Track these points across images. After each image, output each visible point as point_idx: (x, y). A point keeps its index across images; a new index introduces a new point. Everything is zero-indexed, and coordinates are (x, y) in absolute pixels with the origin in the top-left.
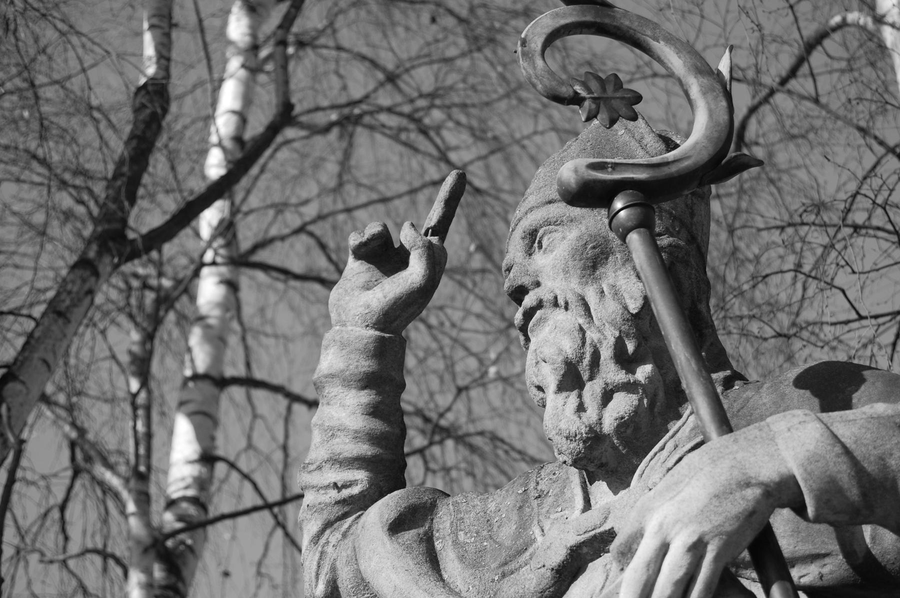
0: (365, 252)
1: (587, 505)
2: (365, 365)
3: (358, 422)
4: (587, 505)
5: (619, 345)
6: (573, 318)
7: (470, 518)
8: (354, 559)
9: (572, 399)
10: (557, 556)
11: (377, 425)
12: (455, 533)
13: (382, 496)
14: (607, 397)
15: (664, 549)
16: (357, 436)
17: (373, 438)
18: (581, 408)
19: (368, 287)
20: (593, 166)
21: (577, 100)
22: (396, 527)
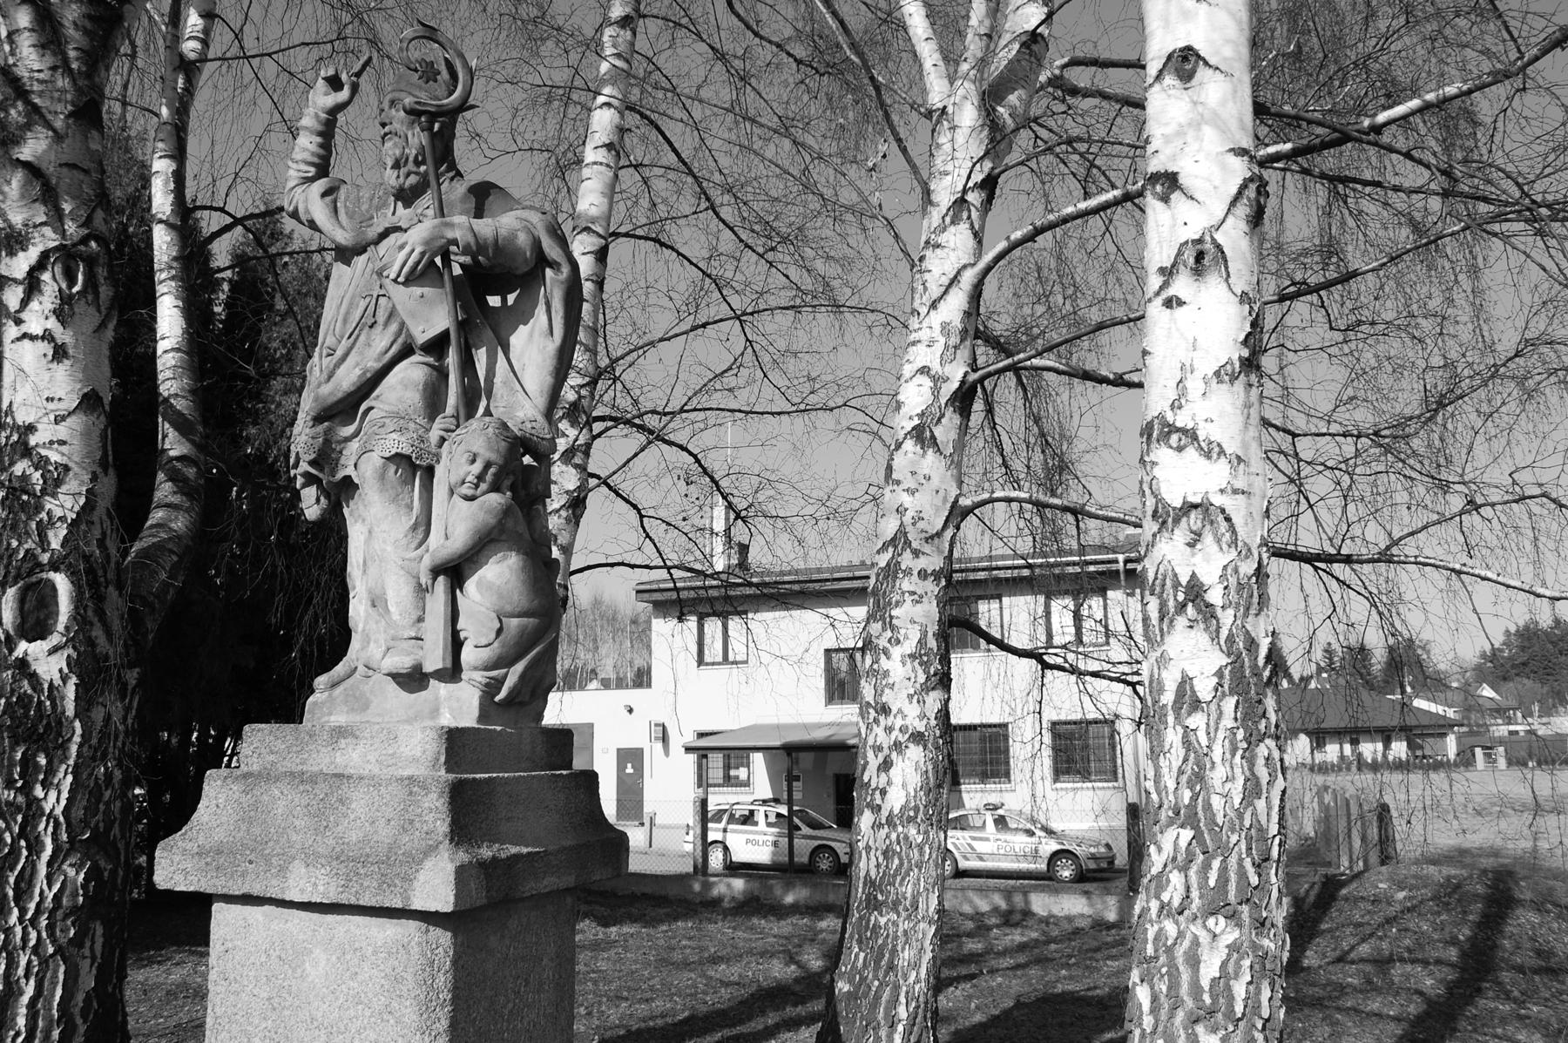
0: (328, 80)
1: (394, 214)
2: (320, 128)
3: (313, 148)
4: (394, 214)
5: (416, 157)
6: (401, 142)
7: (352, 197)
8: (306, 201)
9: (396, 172)
10: (380, 229)
11: (321, 151)
12: (346, 200)
13: (319, 178)
14: (408, 175)
15: (413, 251)
16: (313, 154)
17: (319, 156)
18: (398, 177)
19: (326, 94)
20: (416, 103)
21: (416, 70)
22: (324, 195)
